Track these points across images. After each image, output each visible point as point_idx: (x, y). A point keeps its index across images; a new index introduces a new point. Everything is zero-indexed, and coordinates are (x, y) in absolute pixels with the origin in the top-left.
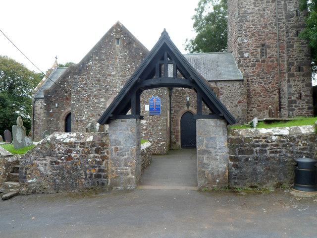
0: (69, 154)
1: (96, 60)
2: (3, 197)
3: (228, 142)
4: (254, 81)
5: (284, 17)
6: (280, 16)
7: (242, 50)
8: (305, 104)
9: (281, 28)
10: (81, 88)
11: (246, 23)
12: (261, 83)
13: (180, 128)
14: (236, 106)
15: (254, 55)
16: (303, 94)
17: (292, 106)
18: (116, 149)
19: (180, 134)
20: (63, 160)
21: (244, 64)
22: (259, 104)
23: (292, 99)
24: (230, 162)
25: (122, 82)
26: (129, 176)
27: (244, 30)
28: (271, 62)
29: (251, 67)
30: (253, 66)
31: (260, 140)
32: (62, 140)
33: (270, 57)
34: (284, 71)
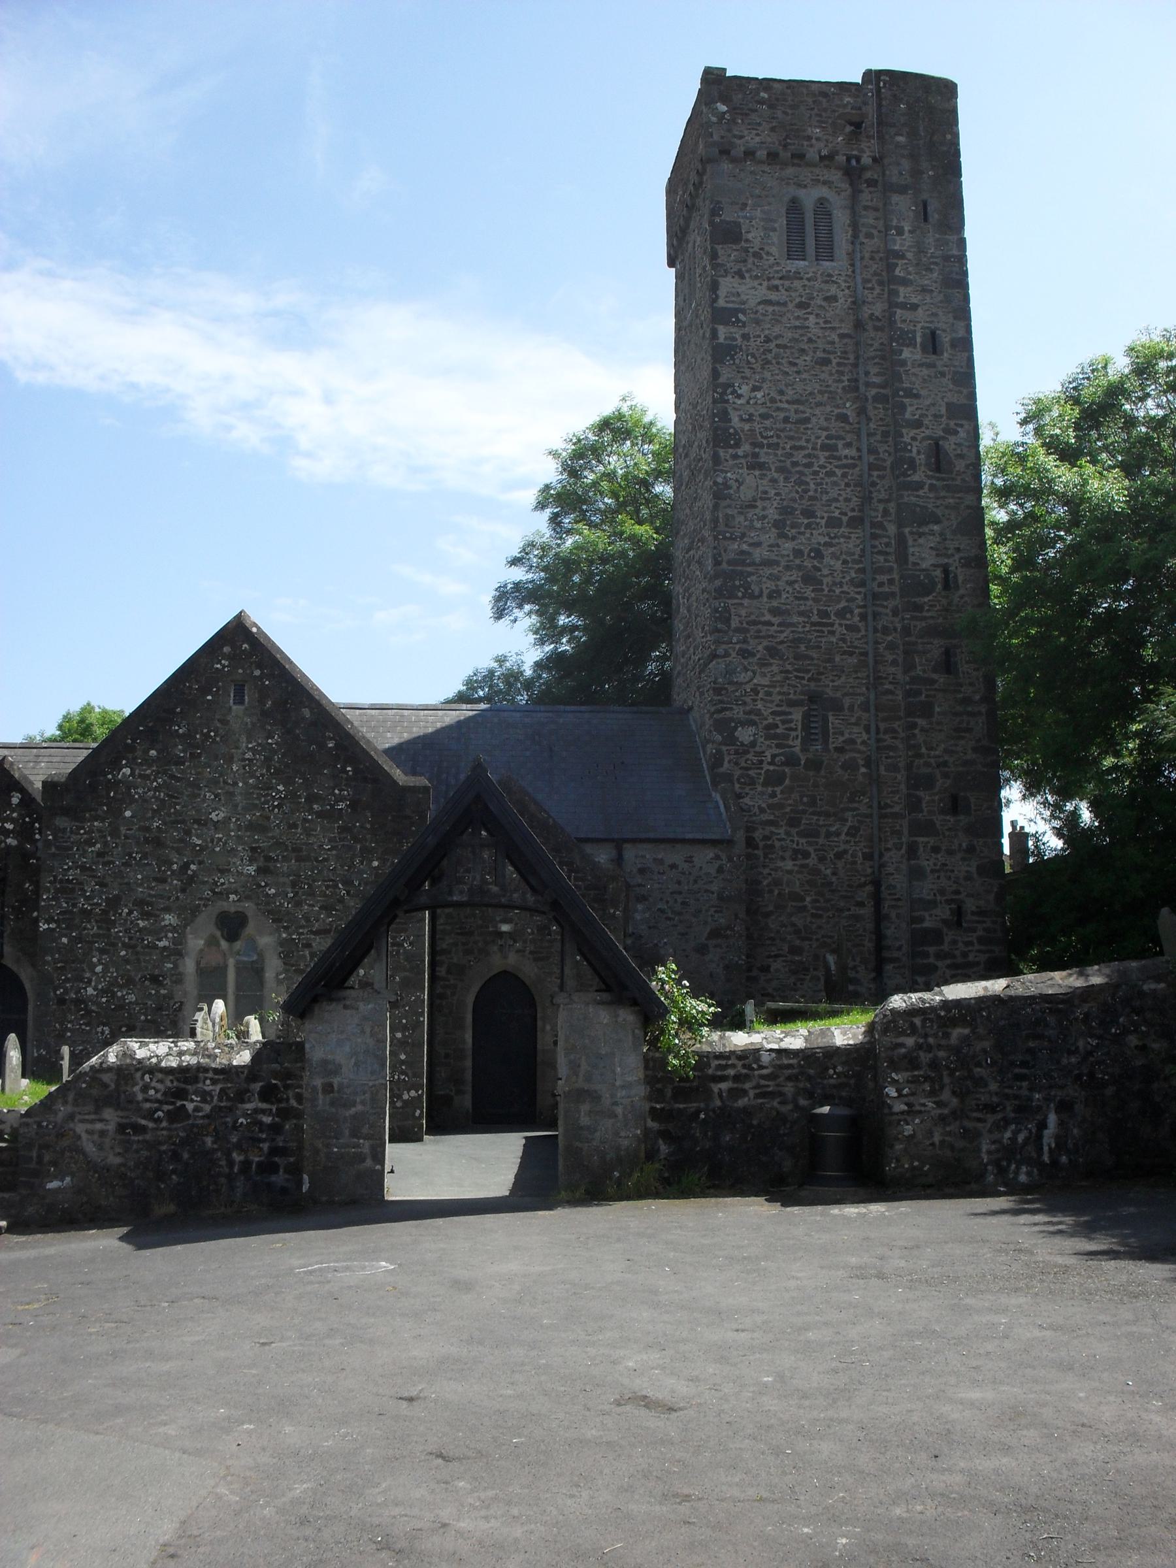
0: (179, 1103)
1: (148, 762)
2: (913, 914)
3: (646, 1068)
4: (777, 844)
5: (895, 589)
6: (881, 584)
7: (728, 714)
8: (977, 947)
9: (886, 630)
10: (83, 868)
11: (746, 602)
12: (806, 855)
13: (468, 1037)
14: (702, 950)
15: (776, 736)
16: (970, 905)
17: (926, 955)
18: (328, 1088)
19: (469, 1063)
20: (159, 1120)
21: (737, 773)
22: (798, 942)
23: (926, 924)
24: (651, 1124)
25: (253, 850)
26: (362, 1166)
27: (737, 630)
28: (845, 767)
29: (765, 784)
30: (774, 779)
31: (730, 1062)
32: (154, 1060)
33: (840, 750)
34: (897, 809)
